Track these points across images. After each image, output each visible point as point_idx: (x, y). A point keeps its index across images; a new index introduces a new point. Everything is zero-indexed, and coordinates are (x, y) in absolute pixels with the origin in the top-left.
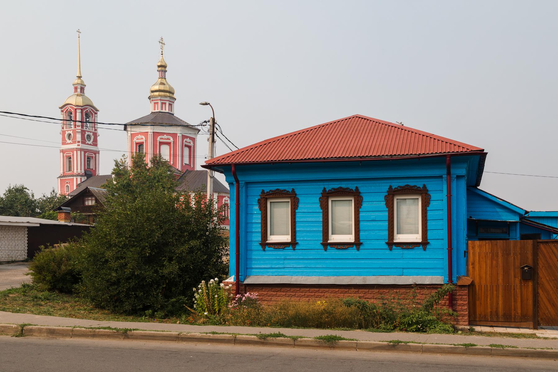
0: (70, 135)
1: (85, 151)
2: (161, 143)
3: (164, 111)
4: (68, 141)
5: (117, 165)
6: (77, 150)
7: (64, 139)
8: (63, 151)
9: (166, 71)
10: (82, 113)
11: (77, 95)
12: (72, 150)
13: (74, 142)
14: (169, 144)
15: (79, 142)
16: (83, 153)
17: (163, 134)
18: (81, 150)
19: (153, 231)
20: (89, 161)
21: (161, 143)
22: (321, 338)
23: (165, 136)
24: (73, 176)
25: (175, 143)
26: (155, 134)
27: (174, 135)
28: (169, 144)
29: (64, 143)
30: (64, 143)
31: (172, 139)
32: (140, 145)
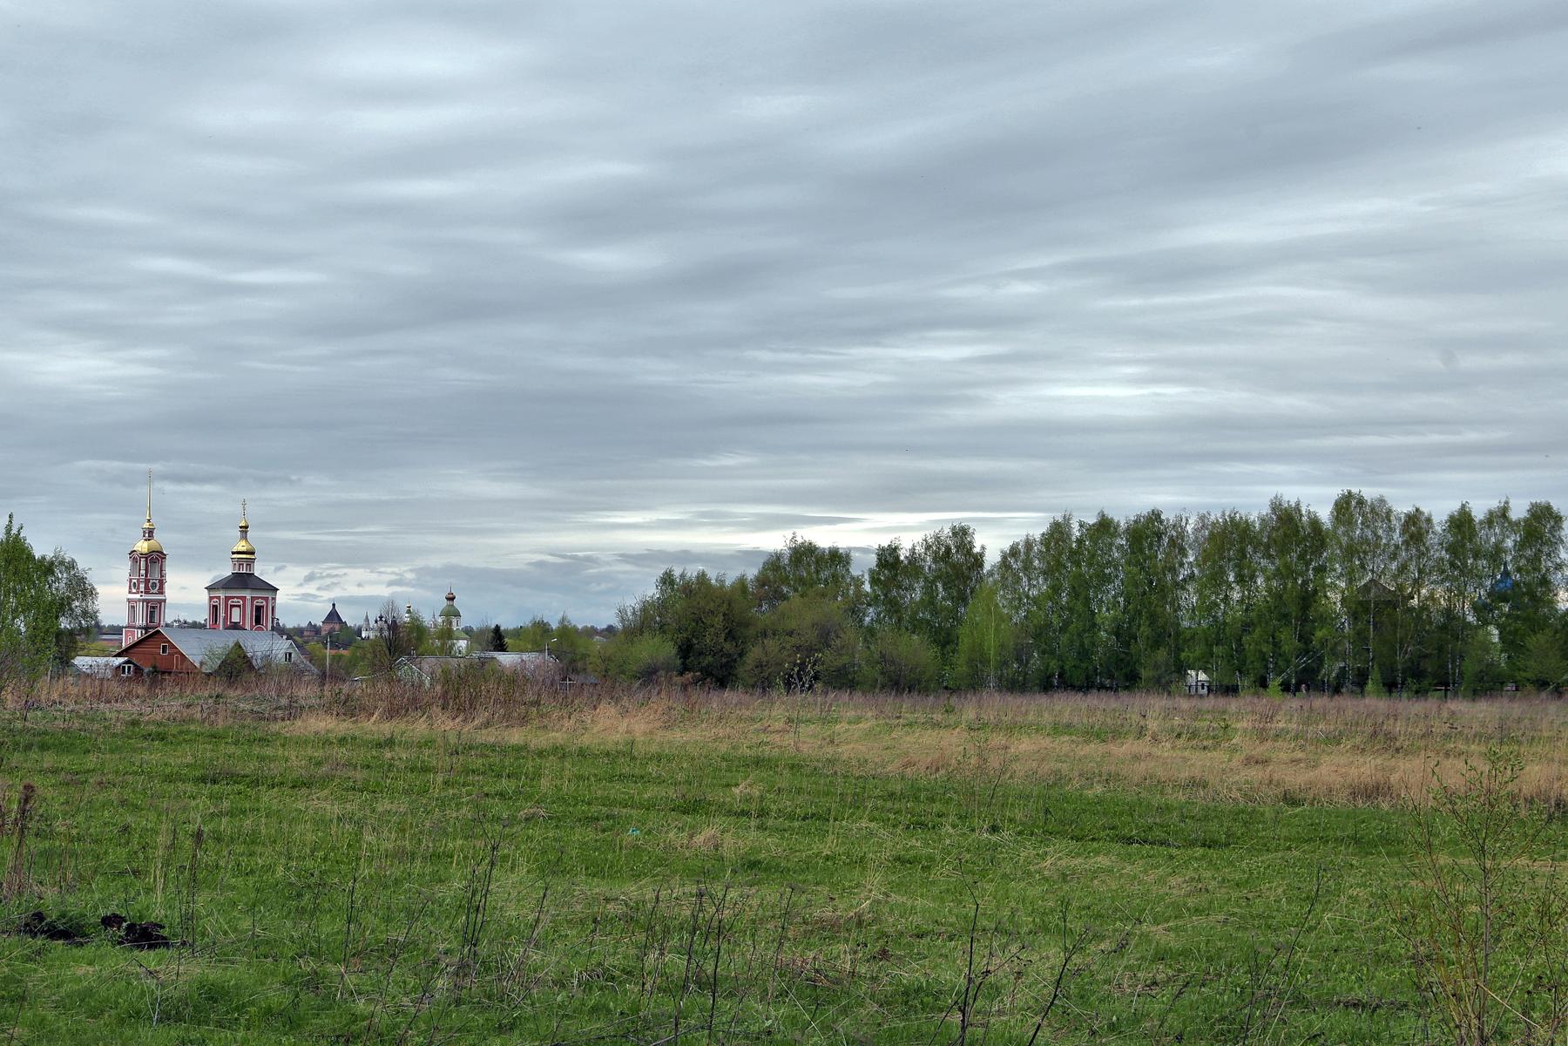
0: (135, 583)
1: (148, 601)
2: (232, 606)
3: (241, 571)
4: (134, 591)
5: (1002, 552)
6: (139, 600)
7: (130, 588)
8: (129, 601)
9: (246, 532)
10: (146, 561)
11: (146, 540)
12: (136, 601)
13: (138, 593)
14: (239, 606)
15: (142, 592)
16: (145, 604)
17: (233, 598)
18: (143, 601)
19: (28, 707)
20: (152, 613)
21: (232, 606)
22: (931, 521)
23: (235, 600)
24: (134, 627)
25: (244, 605)
26: (227, 599)
27: (244, 598)
28: (239, 606)
29: (130, 592)
30: (130, 592)
31: (264, 603)
32: (215, 607)
